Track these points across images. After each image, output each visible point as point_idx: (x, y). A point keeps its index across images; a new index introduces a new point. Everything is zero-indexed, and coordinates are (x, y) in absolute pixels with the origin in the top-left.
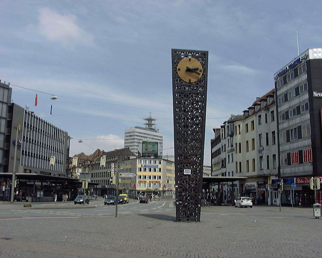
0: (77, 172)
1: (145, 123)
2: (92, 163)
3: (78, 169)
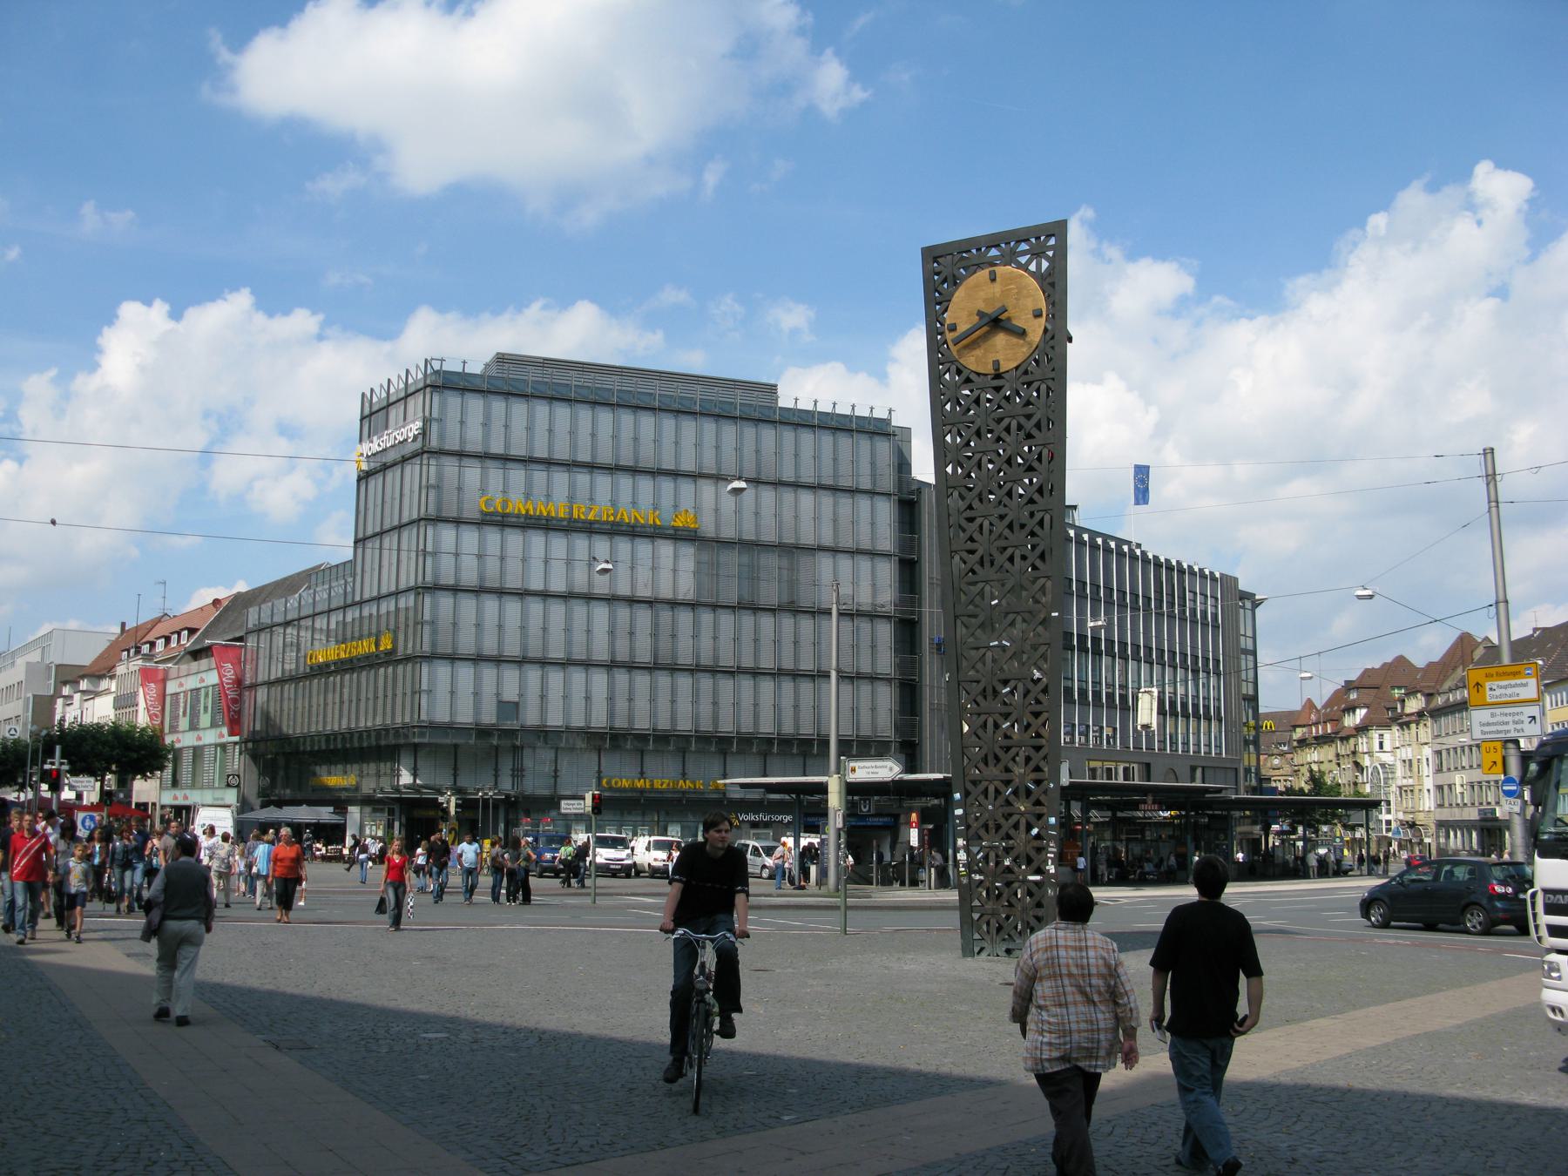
0: (1376, 747)
2: (1432, 706)
3: (1381, 736)
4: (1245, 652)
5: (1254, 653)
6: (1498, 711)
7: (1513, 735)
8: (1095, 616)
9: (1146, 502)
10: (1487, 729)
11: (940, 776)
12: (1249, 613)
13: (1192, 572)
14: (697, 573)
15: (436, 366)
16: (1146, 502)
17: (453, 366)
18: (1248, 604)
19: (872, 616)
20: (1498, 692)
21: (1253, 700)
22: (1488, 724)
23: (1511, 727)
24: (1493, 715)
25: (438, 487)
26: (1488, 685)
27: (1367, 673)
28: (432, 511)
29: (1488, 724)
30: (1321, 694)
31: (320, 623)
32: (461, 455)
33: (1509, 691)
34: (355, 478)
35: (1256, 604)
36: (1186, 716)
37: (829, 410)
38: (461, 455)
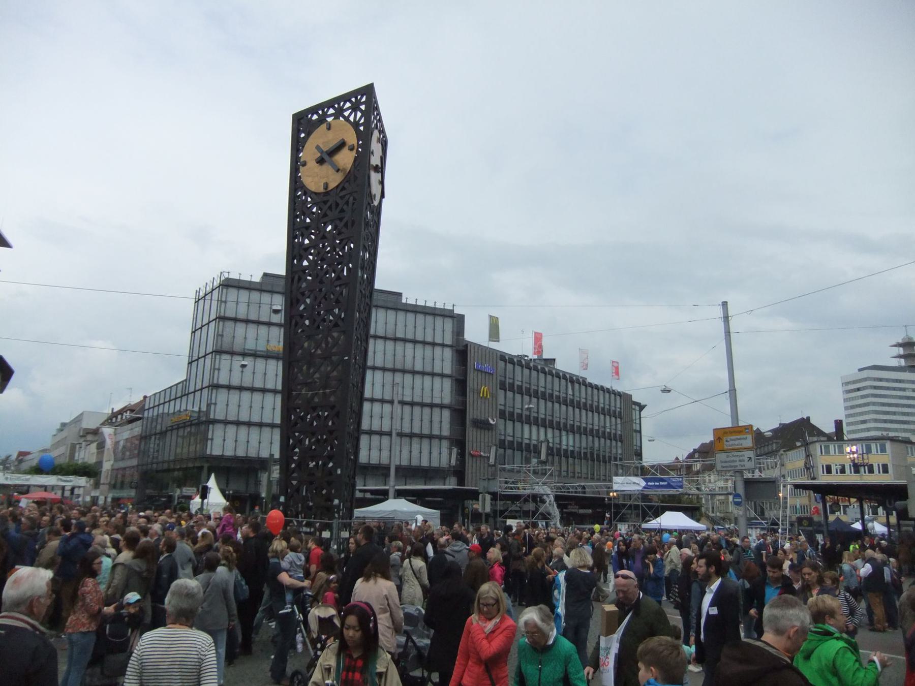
1: (895, 355)
4: (636, 431)
5: (640, 432)
6: (731, 454)
7: (739, 468)
8: (530, 403)
9: (836, 422)
10: (724, 465)
11: (451, 487)
12: (638, 412)
13: (565, 377)
14: (452, 423)
15: (226, 275)
16: (836, 422)
17: (234, 276)
18: (637, 408)
19: (442, 406)
20: (731, 442)
21: (639, 455)
22: (726, 462)
23: (737, 463)
24: (728, 456)
25: (222, 336)
26: (725, 439)
27: (703, 445)
28: (219, 348)
29: (726, 462)
30: (683, 455)
31: (181, 432)
32: (235, 320)
33: (737, 442)
34: (872, 634)
35: (642, 407)
36: (593, 460)
37: (432, 305)
38: (235, 320)
